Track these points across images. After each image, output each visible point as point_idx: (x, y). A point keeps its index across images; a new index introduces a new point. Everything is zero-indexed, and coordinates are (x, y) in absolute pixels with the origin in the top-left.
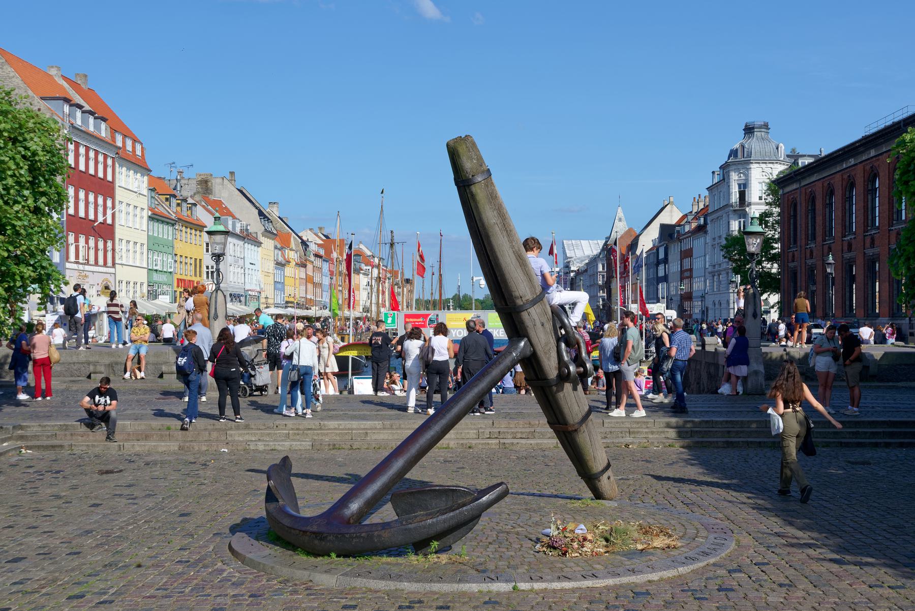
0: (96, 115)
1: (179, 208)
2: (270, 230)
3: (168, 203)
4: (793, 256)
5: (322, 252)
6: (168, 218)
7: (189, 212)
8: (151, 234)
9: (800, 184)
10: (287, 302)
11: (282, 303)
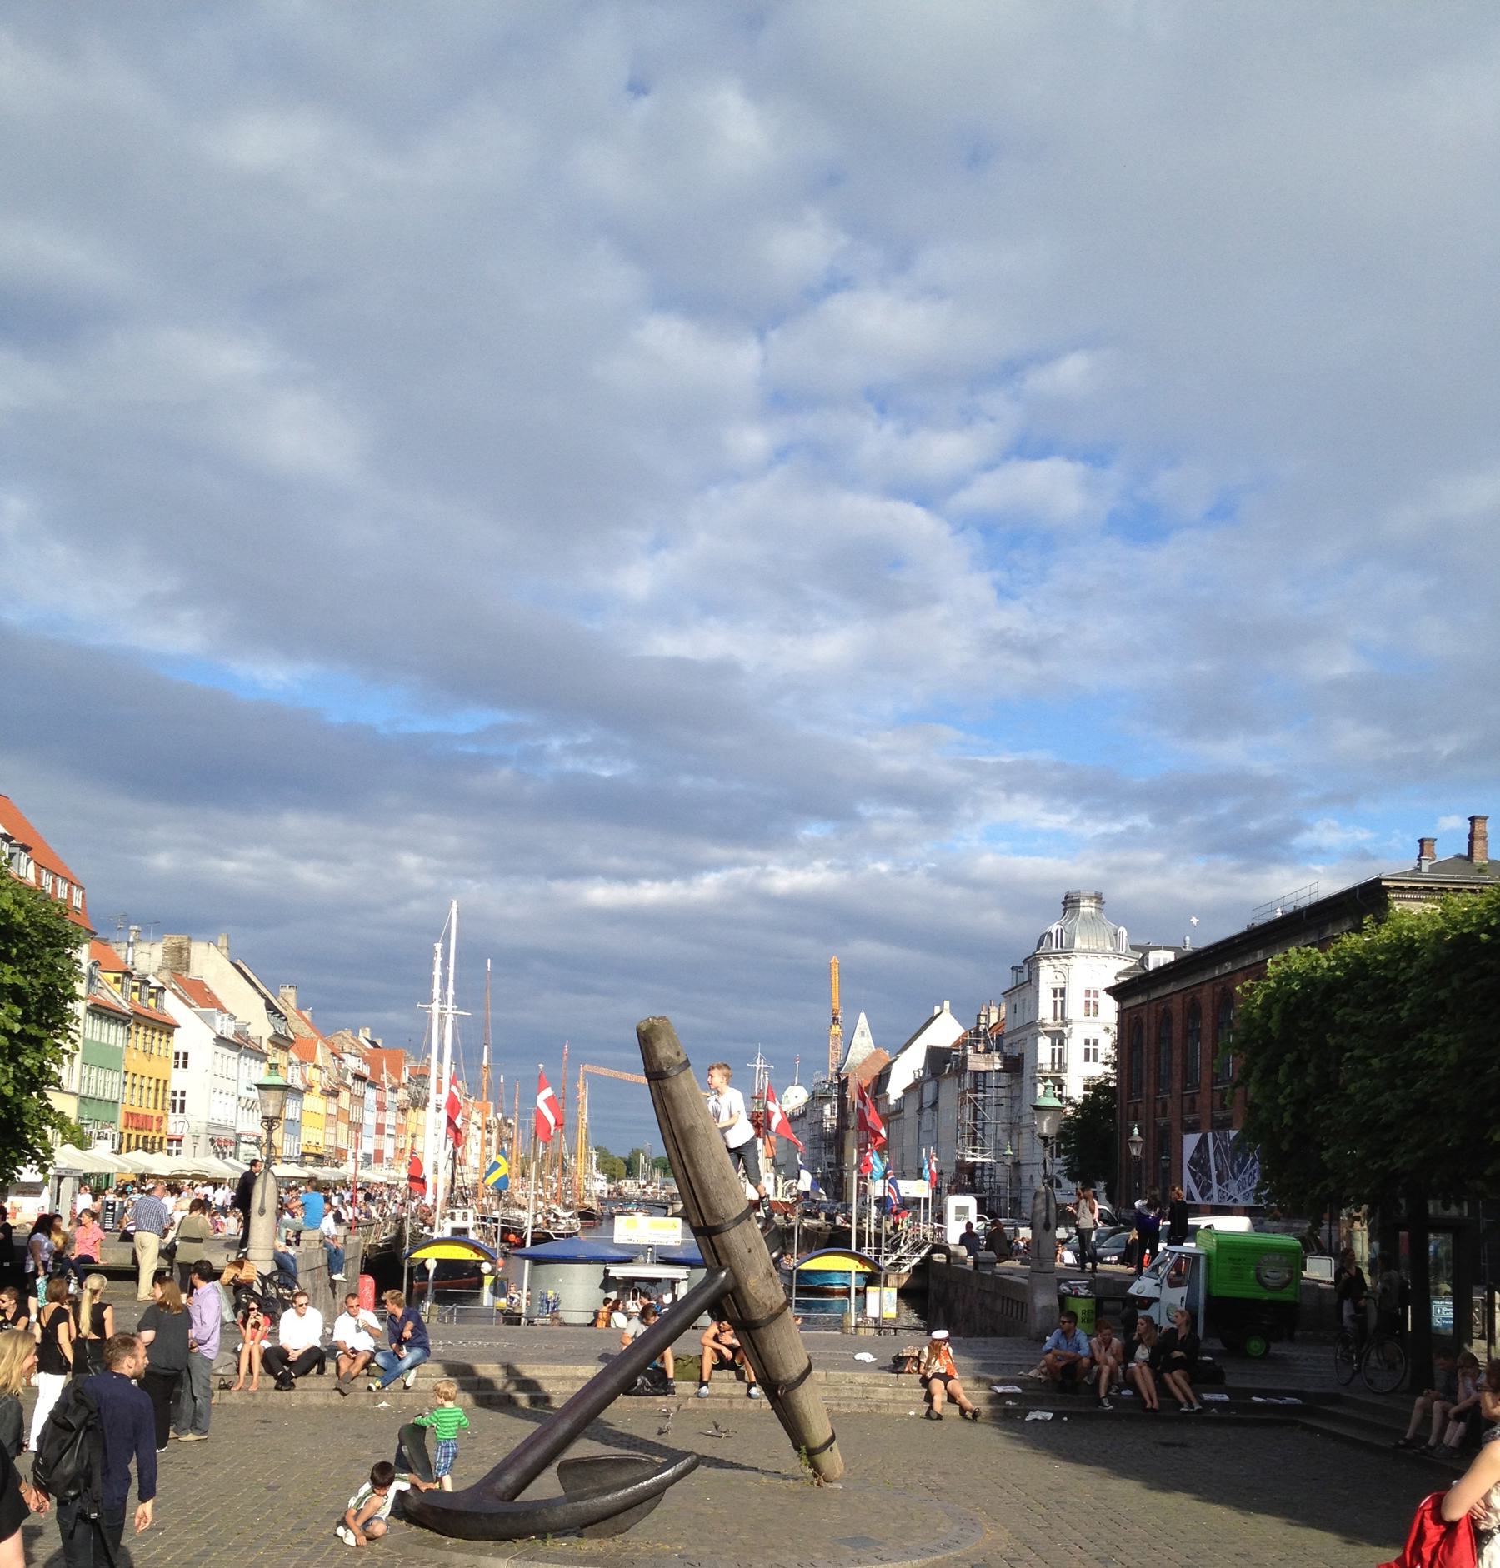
0: (14, 842)
1: (136, 995)
2: (283, 1032)
3: (118, 986)
4: (1136, 1110)
5: (366, 1071)
6: (118, 1012)
7: (152, 1002)
8: (89, 1036)
9: (1148, 996)
10: (304, 1155)
11: (296, 1155)
